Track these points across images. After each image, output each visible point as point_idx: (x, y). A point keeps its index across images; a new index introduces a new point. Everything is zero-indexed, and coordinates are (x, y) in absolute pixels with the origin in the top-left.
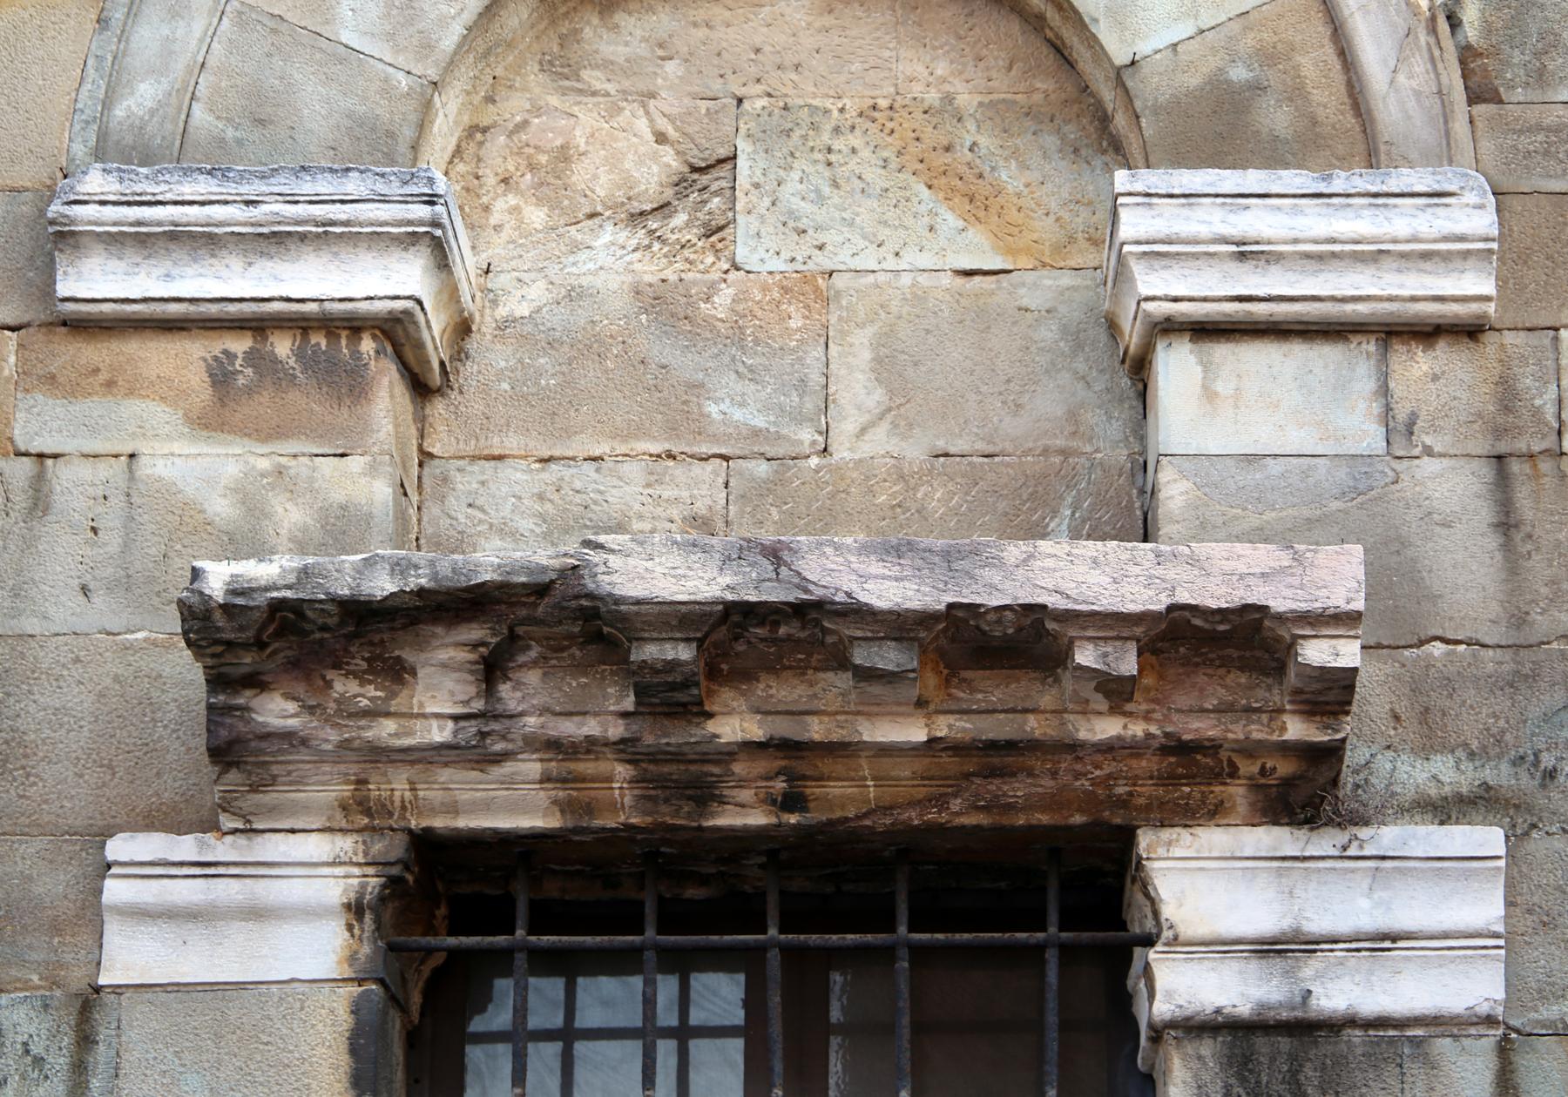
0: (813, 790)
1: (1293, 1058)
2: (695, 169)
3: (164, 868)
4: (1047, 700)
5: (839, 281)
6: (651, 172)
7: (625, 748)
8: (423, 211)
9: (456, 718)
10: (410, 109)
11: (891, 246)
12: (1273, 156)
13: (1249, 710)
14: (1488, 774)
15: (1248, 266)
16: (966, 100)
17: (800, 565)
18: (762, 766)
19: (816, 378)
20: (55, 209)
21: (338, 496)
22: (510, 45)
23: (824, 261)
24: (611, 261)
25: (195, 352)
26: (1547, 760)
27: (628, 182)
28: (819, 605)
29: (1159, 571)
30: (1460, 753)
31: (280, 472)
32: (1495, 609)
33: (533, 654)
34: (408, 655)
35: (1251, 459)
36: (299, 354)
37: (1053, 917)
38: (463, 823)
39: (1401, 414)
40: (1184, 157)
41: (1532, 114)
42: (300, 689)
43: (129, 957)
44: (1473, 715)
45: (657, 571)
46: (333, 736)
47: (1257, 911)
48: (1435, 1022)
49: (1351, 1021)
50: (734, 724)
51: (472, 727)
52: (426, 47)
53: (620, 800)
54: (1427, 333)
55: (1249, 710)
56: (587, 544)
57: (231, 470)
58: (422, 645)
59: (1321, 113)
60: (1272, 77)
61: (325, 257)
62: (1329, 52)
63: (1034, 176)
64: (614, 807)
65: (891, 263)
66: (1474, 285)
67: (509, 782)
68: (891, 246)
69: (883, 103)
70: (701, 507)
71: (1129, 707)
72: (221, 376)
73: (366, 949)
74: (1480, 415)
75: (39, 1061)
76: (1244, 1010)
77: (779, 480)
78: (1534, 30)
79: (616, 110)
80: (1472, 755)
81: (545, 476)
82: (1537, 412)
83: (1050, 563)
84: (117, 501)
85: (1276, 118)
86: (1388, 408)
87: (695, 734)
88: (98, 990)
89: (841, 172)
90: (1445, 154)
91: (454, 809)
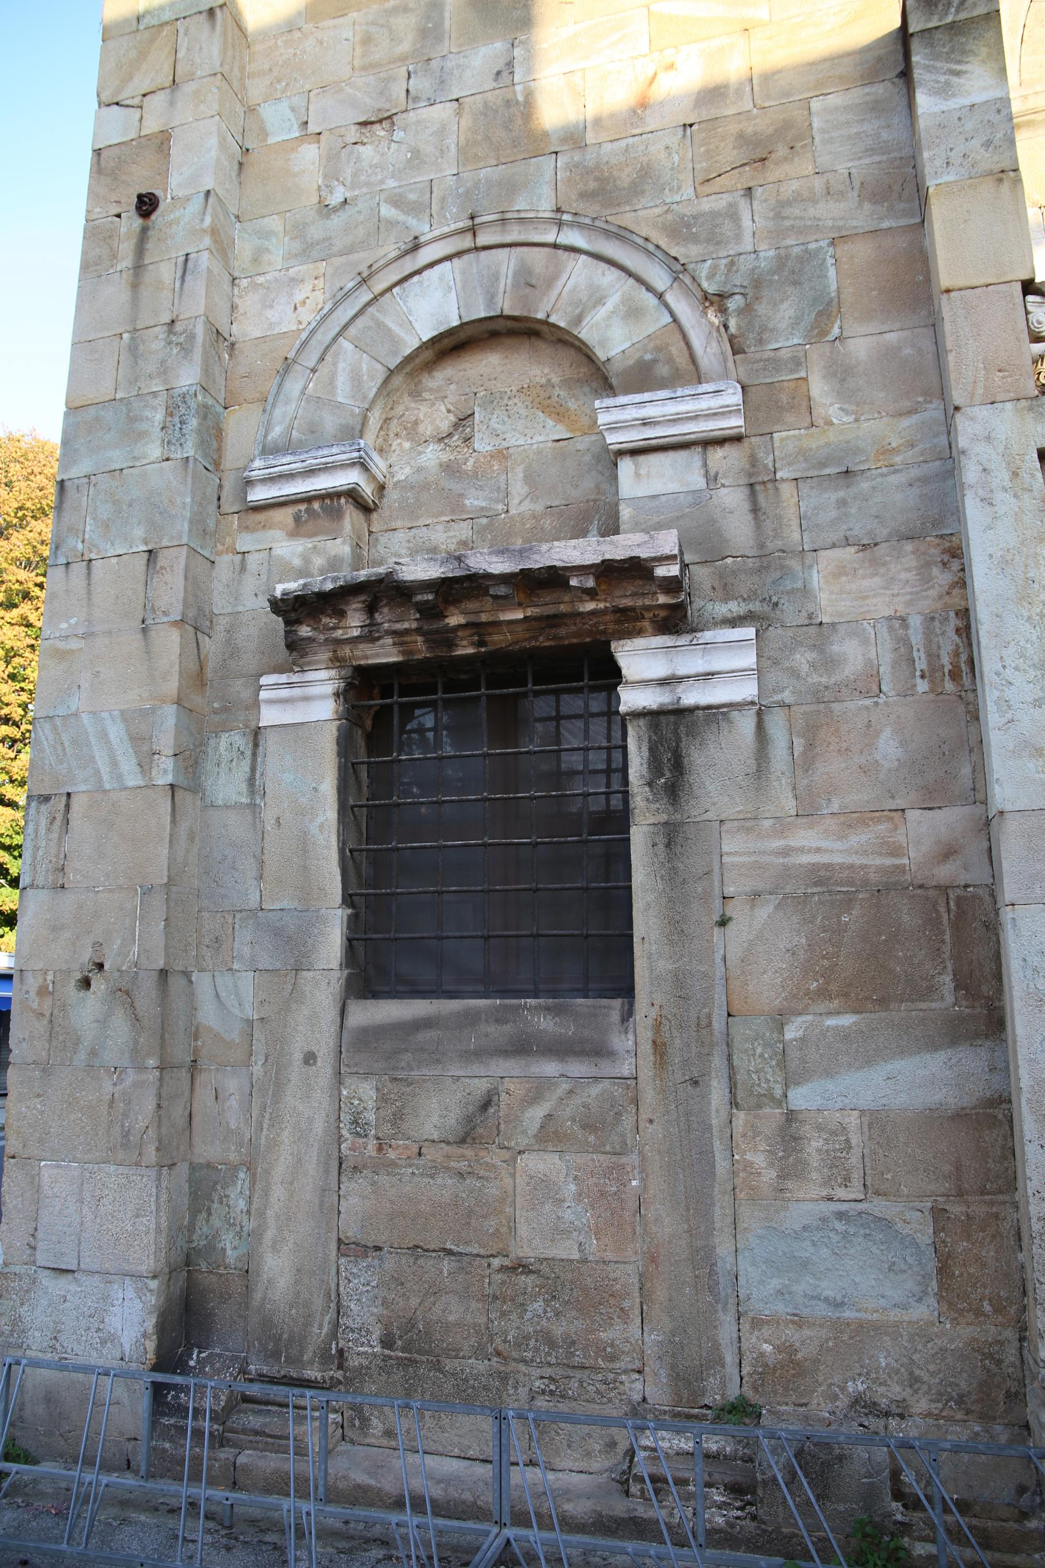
0: (488, 639)
1: (675, 723)
2: (460, 420)
3: (277, 686)
4: (567, 598)
5: (511, 451)
6: (445, 423)
7: (418, 631)
8: (356, 454)
9: (361, 627)
10: (359, 420)
11: (529, 436)
12: (662, 384)
13: (643, 594)
14: (751, 607)
15: (648, 427)
16: (555, 380)
17: (468, 561)
18: (468, 632)
19: (503, 486)
20: (246, 473)
21: (333, 553)
22: (397, 390)
23: (505, 444)
24: (432, 456)
25: (289, 512)
26: (774, 599)
27: (438, 428)
28: (475, 575)
29: (599, 548)
30: (740, 600)
31: (315, 547)
32: (752, 542)
33: (385, 602)
34: (343, 607)
35: (654, 497)
36: (321, 507)
37: (586, 676)
38: (370, 662)
39: (712, 473)
40: (627, 391)
41: (758, 356)
42: (312, 622)
43: (269, 716)
44: (745, 584)
45: (419, 570)
46: (322, 637)
47: (659, 669)
48: (731, 705)
49: (697, 708)
50: (454, 620)
51: (366, 630)
52: (365, 397)
53: (421, 649)
54: (720, 442)
55: (643, 594)
56: (396, 563)
57: (300, 549)
58: (347, 604)
59: (680, 366)
60: (661, 356)
61: (327, 474)
62: (682, 344)
63: (581, 402)
64: (419, 652)
65: (530, 441)
66: (735, 423)
67: (382, 646)
68: (529, 436)
69: (526, 386)
70: (464, 538)
71: (598, 597)
72: (297, 519)
73: (341, 708)
74: (742, 470)
75: (242, 753)
76: (655, 707)
77: (491, 524)
78: (757, 325)
79: (433, 405)
80: (744, 600)
81: (411, 534)
82: (766, 466)
83: (558, 550)
84: (266, 564)
85: (663, 370)
86: (707, 471)
87: (441, 624)
88: (259, 728)
89: (511, 412)
90: (725, 375)
91: (366, 657)
